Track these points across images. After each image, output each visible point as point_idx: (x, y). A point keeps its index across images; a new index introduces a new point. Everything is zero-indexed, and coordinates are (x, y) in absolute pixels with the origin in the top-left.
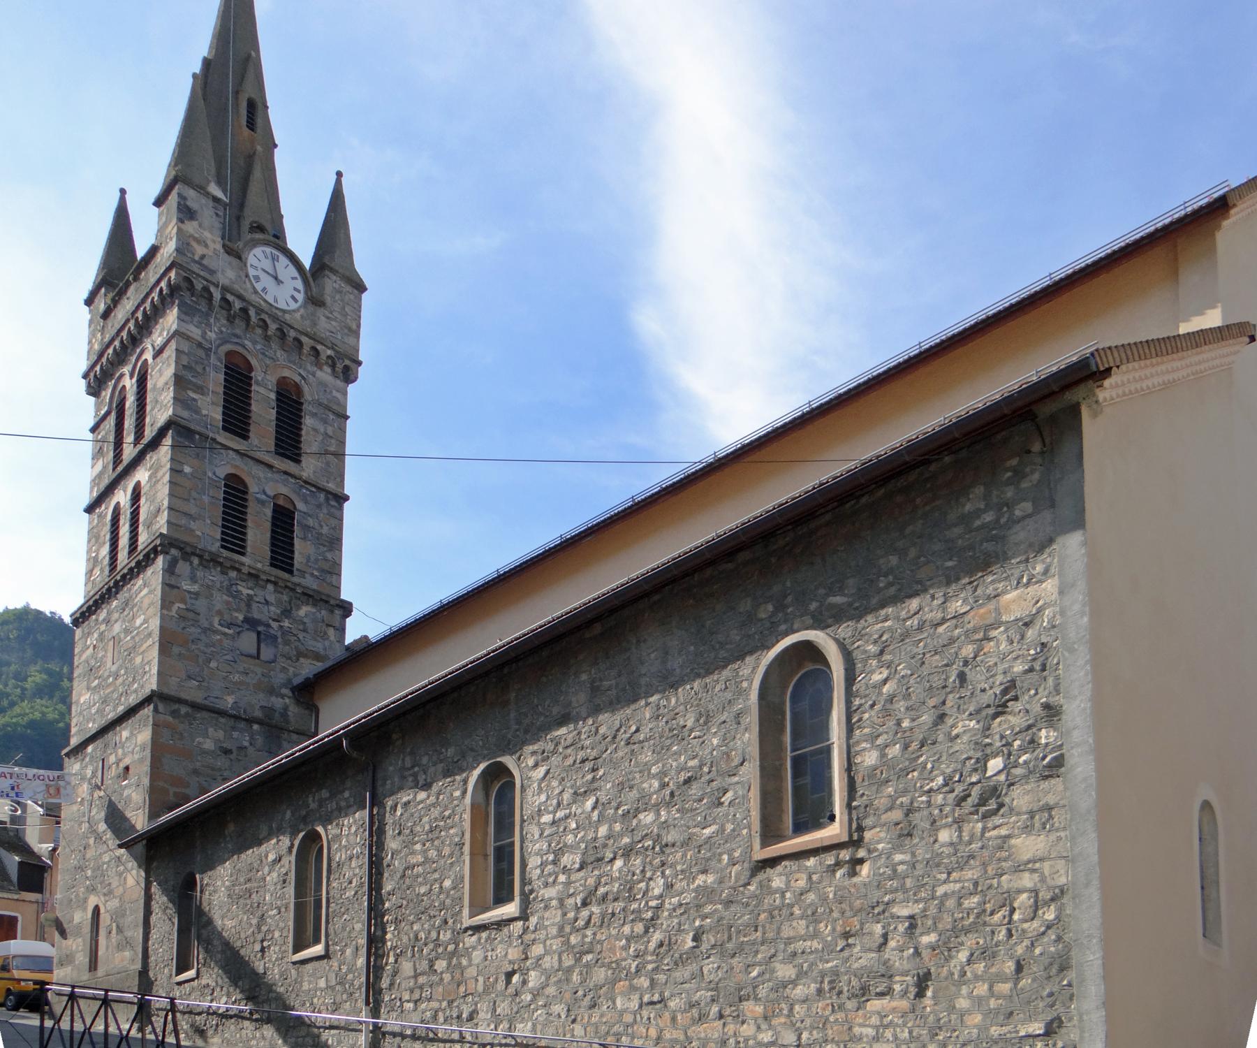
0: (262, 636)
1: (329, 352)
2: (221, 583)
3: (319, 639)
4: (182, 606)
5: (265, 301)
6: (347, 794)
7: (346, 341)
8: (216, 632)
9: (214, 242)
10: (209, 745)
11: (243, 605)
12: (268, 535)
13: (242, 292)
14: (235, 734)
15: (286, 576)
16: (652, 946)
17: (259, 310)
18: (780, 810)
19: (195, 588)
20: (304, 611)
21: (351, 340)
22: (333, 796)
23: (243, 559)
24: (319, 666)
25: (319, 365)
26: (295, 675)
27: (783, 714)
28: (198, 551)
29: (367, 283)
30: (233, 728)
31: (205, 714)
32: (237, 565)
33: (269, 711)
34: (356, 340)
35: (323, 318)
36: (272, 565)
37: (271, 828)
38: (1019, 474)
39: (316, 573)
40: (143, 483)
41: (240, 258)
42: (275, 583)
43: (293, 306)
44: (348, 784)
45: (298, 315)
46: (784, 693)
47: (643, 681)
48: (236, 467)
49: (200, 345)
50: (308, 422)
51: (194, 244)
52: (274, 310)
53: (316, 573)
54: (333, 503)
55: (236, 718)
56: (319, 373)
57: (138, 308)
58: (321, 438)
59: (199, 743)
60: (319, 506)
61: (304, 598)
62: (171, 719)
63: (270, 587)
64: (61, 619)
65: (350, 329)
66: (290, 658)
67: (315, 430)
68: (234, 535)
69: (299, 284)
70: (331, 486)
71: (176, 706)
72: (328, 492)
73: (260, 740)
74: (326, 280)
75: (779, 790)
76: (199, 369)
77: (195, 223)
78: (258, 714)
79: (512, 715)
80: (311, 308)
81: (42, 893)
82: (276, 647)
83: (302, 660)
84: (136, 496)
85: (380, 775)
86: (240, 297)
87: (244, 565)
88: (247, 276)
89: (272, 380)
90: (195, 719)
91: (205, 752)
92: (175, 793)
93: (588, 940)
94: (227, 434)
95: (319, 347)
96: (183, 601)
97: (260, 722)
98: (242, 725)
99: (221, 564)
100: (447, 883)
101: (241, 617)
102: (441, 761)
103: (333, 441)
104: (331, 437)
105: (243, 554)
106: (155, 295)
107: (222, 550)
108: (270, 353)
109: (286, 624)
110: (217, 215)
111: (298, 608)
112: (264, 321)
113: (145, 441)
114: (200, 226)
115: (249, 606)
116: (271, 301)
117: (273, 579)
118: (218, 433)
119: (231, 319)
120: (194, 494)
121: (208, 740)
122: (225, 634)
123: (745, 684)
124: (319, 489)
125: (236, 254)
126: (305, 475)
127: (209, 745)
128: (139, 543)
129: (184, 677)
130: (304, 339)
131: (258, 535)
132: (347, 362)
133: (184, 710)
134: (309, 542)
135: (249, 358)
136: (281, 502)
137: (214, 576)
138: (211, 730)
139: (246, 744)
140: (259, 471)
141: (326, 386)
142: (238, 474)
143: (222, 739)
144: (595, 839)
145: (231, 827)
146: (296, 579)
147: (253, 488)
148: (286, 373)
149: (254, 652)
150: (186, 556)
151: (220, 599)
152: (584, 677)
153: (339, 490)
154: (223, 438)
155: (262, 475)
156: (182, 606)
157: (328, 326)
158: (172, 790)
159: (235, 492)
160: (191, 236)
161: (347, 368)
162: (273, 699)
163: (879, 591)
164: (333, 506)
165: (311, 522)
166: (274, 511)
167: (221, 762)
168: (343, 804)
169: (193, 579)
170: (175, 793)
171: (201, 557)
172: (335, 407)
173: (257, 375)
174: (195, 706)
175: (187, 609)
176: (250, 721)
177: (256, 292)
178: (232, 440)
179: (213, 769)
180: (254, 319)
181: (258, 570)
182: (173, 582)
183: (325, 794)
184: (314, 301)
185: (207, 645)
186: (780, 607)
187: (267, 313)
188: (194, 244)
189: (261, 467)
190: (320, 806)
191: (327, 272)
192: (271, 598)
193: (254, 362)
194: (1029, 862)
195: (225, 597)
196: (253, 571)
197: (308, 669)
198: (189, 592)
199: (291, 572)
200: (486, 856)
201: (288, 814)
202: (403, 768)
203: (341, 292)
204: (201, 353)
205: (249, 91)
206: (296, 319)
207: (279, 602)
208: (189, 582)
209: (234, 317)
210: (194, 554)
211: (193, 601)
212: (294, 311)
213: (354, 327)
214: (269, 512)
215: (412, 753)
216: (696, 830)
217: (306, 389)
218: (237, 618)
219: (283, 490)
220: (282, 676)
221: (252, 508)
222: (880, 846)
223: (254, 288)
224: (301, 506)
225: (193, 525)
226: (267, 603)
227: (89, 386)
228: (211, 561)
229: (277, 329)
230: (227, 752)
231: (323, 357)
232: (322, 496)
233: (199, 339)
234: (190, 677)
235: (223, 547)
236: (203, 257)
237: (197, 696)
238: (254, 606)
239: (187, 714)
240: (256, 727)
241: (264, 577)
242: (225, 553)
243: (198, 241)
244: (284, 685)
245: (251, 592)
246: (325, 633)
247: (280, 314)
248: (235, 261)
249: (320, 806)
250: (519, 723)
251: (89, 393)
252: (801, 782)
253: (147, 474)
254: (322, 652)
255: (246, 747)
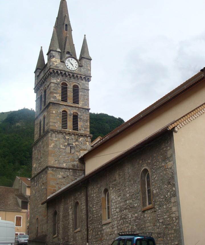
0: (72, 147)
1: (84, 76)
2: (62, 136)
3: (85, 145)
4: (54, 144)
5: (70, 70)
6: (83, 194)
7: (88, 72)
8: (61, 149)
9: (58, 61)
10: (60, 177)
11: (67, 141)
12: (72, 123)
13: (64, 69)
14: (66, 173)
15: (76, 131)
16: (130, 228)
17: (68, 72)
18: (146, 201)
19: (57, 139)
20: (81, 139)
21: (89, 72)
22: (80, 194)
23: (67, 130)
24: (86, 152)
25: (82, 80)
26: (79, 155)
27: (145, 181)
28: (57, 131)
29: (92, 58)
30: (66, 171)
31: (59, 169)
32: (65, 132)
33: (74, 166)
34: (90, 72)
35: (82, 69)
36: (73, 129)
37: (70, 201)
38: (168, 142)
39: (83, 129)
40: (46, 115)
41: (64, 62)
42: (74, 134)
43: (76, 69)
44: (83, 191)
45: (77, 71)
46: (145, 178)
47: (126, 174)
48: (65, 109)
49: (56, 83)
50: (80, 93)
51: (54, 63)
52: (71, 71)
53: (83, 129)
54: (86, 111)
55: (66, 169)
56: (82, 82)
57: (44, 76)
58: (83, 96)
59: (58, 176)
60: (83, 113)
61: (80, 136)
62: (52, 172)
63: (73, 135)
64: (34, 110)
65: (89, 70)
66: (78, 152)
67: (82, 95)
68: (64, 125)
69: (77, 64)
70: (86, 107)
71: (53, 168)
72: (85, 109)
73: (72, 174)
74: (83, 60)
75: (145, 197)
76: (56, 89)
77: (55, 58)
78: (71, 167)
79: (108, 179)
80: (79, 68)
81: (27, 209)
82: (75, 149)
83: (81, 151)
84: (44, 118)
85: (88, 190)
86: (64, 71)
87: (67, 131)
88: (66, 66)
89: (72, 86)
90: (57, 171)
91: (59, 178)
92: (53, 190)
93: (121, 227)
94: (63, 102)
95: (82, 76)
96: (54, 143)
97: (72, 169)
98: (68, 170)
99: (62, 132)
100: (99, 215)
101: (67, 144)
102: (98, 188)
103: (86, 96)
104: (85, 95)
105: (67, 129)
106: (47, 74)
107: (62, 129)
108: (71, 80)
109: (77, 143)
110: (59, 55)
111: (80, 139)
112: (69, 74)
113: (46, 105)
114: (56, 58)
115: (68, 141)
116: (71, 69)
117: (73, 133)
118: (61, 102)
119: (62, 76)
120: (56, 117)
121: (60, 175)
122: (63, 149)
123: (139, 176)
124: (83, 109)
125: (63, 62)
126: (80, 106)
127: (60, 177)
128: (45, 129)
129: (54, 161)
130: (78, 75)
131: (70, 123)
132: (88, 77)
133: (55, 169)
134: (81, 122)
135: (67, 83)
136: (75, 114)
137: (60, 136)
138: (61, 173)
139: (69, 175)
140: (69, 108)
141: (84, 84)
142: (65, 110)
143: (63, 174)
144: (121, 206)
145: (63, 200)
146: (79, 132)
147: (69, 113)
148: (75, 84)
149: (70, 152)
150: (54, 132)
151: (62, 140)
152: (118, 172)
153: (88, 108)
154: (62, 103)
155: (70, 109)
156: (54, 144)
157: (83, 71)
158: (52, 189)
159: (65, 113)
160: (54, 61)
161: (88, 78)
162: (75, 162)
163: (154, 160)
164: (86, 112)
165: (82, 117)
166: (73, 117)
167: (63, 180)
168: (82, 196)
169: (56, 137)
170: (53, 190)
171: (57, 132)
172: (86, 88)
173: (68, 86)
174: (57, 168)
175: (55, 145)
176: (69, 169)
177: (67, 68)
178: (63, 103)
179: (61, 182)
180: (67, 74)
181: (70, 132)
182: (52, 139)
183: (79, 193)
184: (80, 66)
185: (59, 152)
186: (142, 162)
187: (70, 72)
188: (54, 63)
189: (70, 107)
190: (78, 196)
191: (83, 59)
192: (73, 138)
193: (67, 84)
194: (174, 212)
195: (63, 140)
196: (69, 132)
197: (82, 154)
198: (55, 141)
199: (78, 130)
200: (106, 208)
201: (73, 198)
202: (91, 189)
203: (86, 62)
204: (56, 85)
205: (66, 23)
206: (77, 72)
207: (75, 138)
208: (55, 138)
209: (63, 75)
210: (56, 132)
211: (56, 142)
212: (76, 70)
213: (90, 69)
214: (72, 117)
215: (93, 185)
216: (134, 205)
217: (79, 86)
218: (66, 144)
219: (75, 111)
220: (77, 156)
221: (68, 116)
222: (157, 209)
223: (67, 67)
224: (79, 114)
225: (55, 124)
226: (72, 139)
227: (35, 91)
228: (60, 132)
229: (72, 75)
230: (64, 177)
231: (83, 78)
232: (84, 110)
233: (56, 82)
234: (56, 161)
235: (62, 128)
236: (56, 65)
237: (58, 166)
238: (69, 140)
239: (55, 170)
240: (71, 170)
241: (71, 133)
242: (63, 129)
243: (55, 62)
244: (77, 159)
245: (69, 137)
246: (86, 144)
247: (73, 71)
248: (63, 63)
249: (78, 196)
250: (109, 180)
251: (35, 93)
252: (150, 194)
253: (46, 113)
254: (86, 148)
255: (68, 176)
